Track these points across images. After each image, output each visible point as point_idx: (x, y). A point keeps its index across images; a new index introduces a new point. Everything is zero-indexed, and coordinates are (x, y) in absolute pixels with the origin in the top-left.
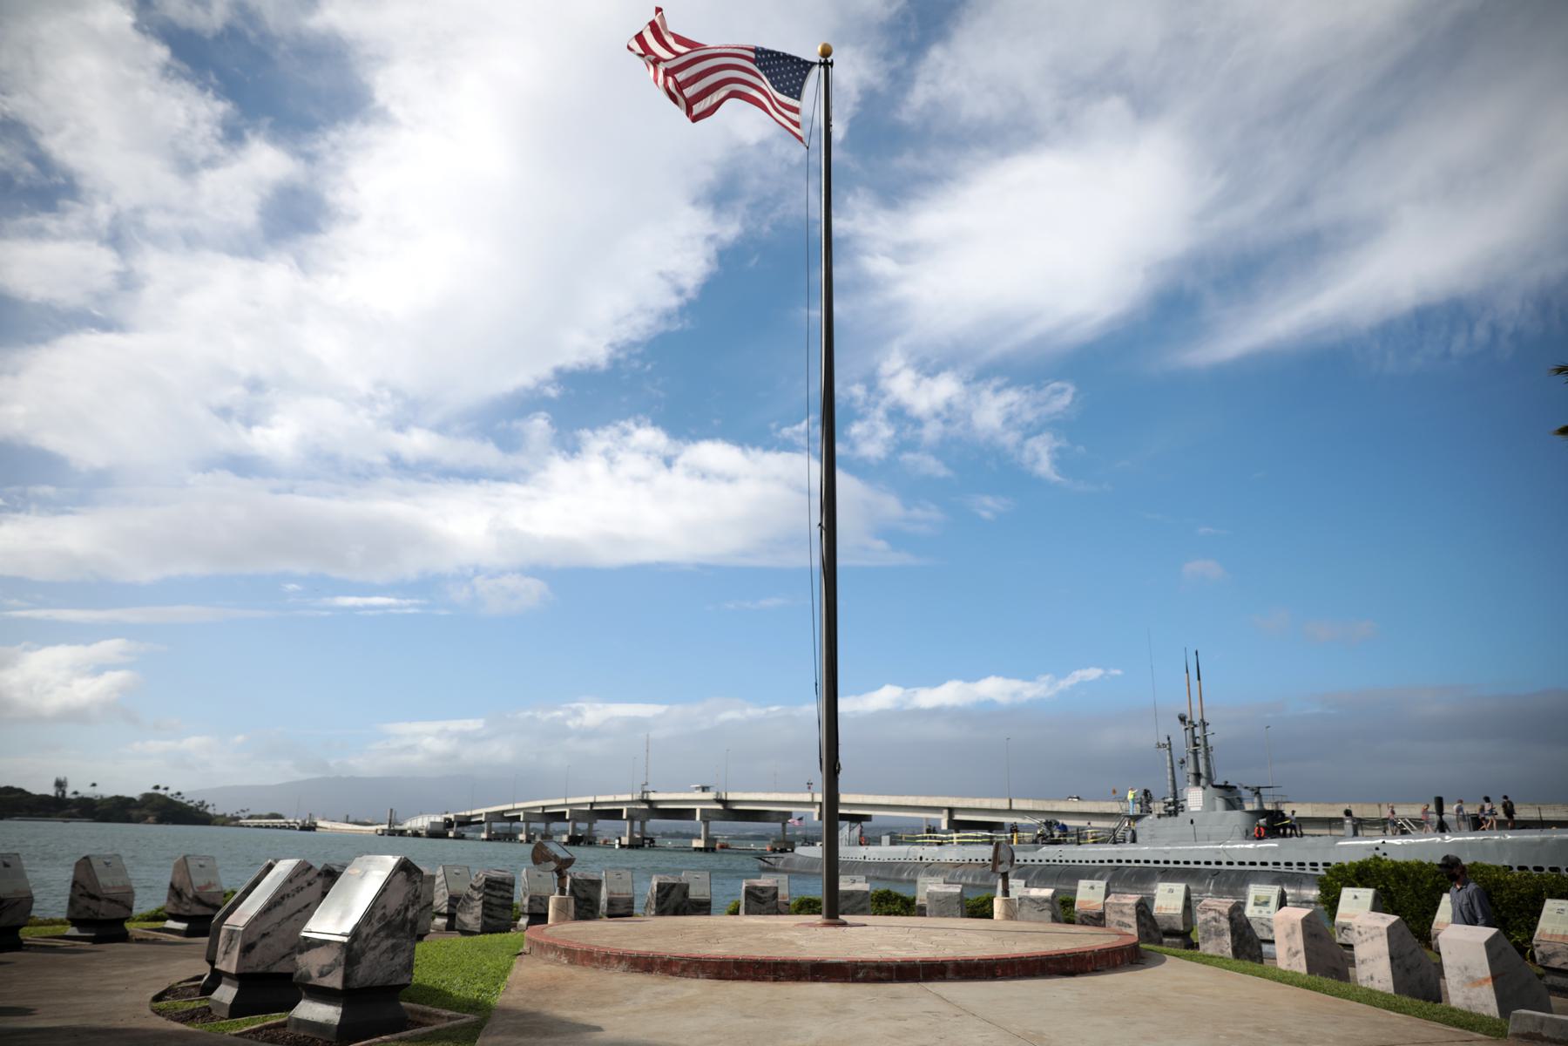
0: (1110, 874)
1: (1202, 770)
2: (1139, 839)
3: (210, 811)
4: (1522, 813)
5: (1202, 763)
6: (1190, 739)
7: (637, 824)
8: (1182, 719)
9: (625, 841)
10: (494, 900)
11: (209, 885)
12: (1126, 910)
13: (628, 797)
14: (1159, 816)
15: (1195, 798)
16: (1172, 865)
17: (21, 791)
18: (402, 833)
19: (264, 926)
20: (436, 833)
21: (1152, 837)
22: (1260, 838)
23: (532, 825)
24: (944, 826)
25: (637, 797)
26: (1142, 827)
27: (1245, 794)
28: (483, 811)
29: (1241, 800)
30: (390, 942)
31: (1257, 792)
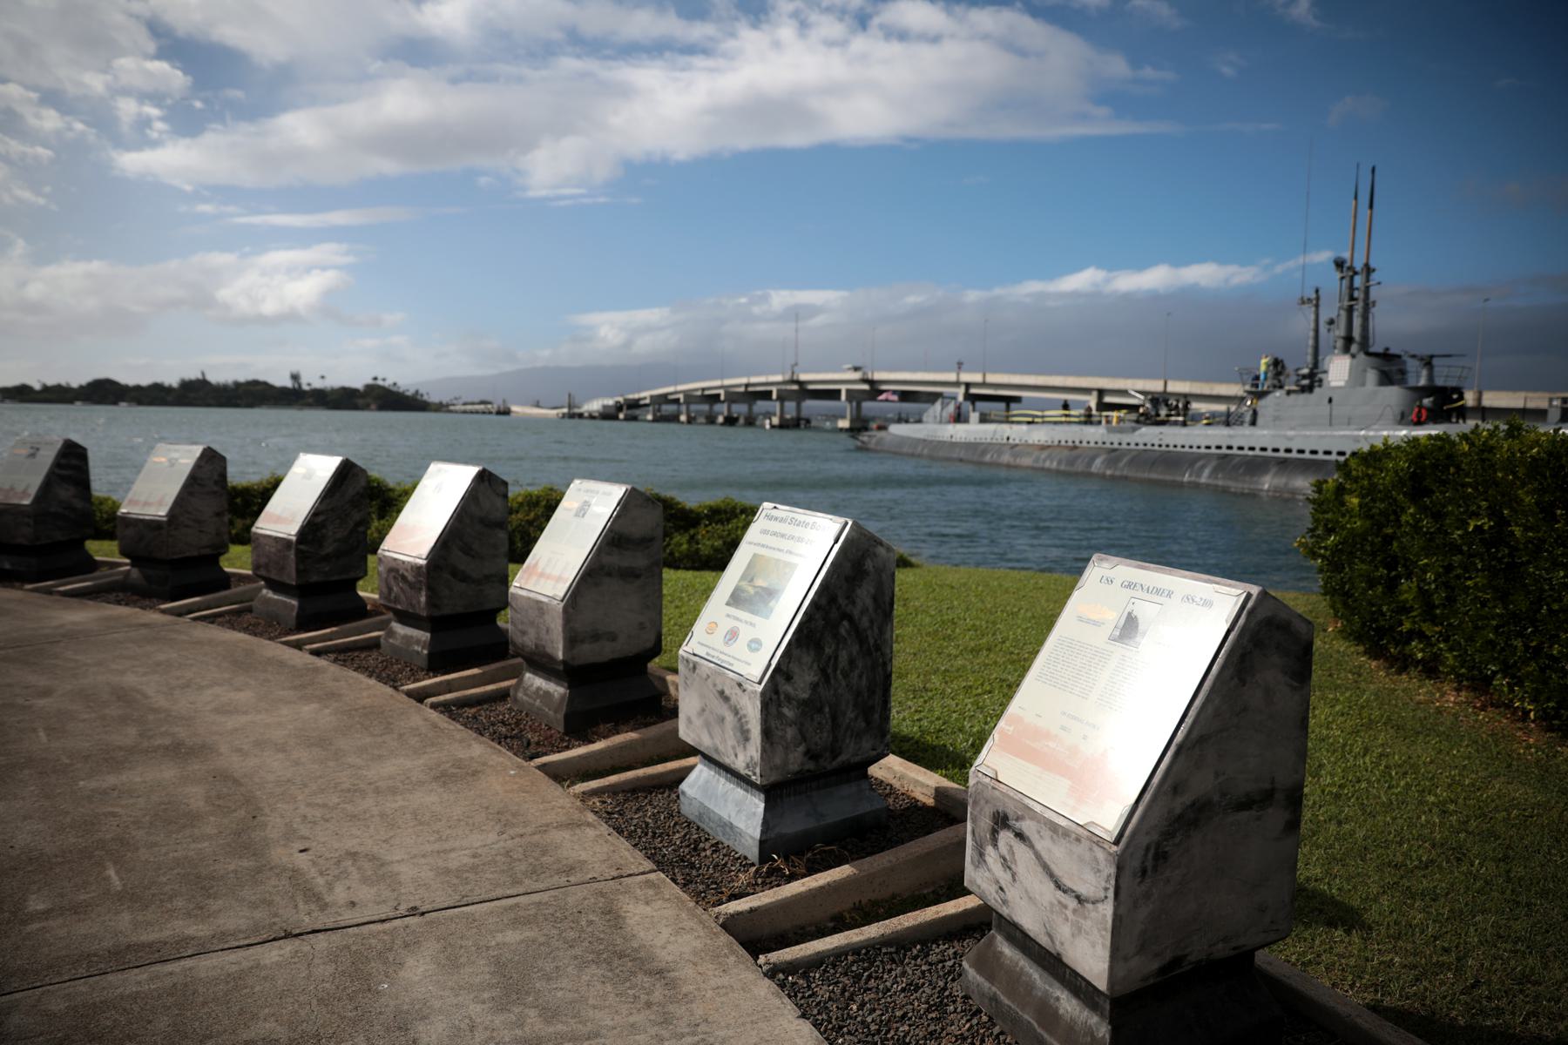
0: (1214, 463)
1: (1356, 333)
2: (1260, 421)
5: (1357, 322)
6: (1345, 291)
8: (1339, 264)
9: (776, 421)
13: (779, 378)
15: (1338, 370)
16: (1294, 455)
17: (265, 384)
18: (581, 416)
20: (608, 415)
21: (1276, 418)
22: (1418, 423)
23: (693, 407)
24: (961, 398)
25: (788, 377)
26: (1267, 406)
27: (1412, 365)
29: (1403, 372)
31: (1428, 362)
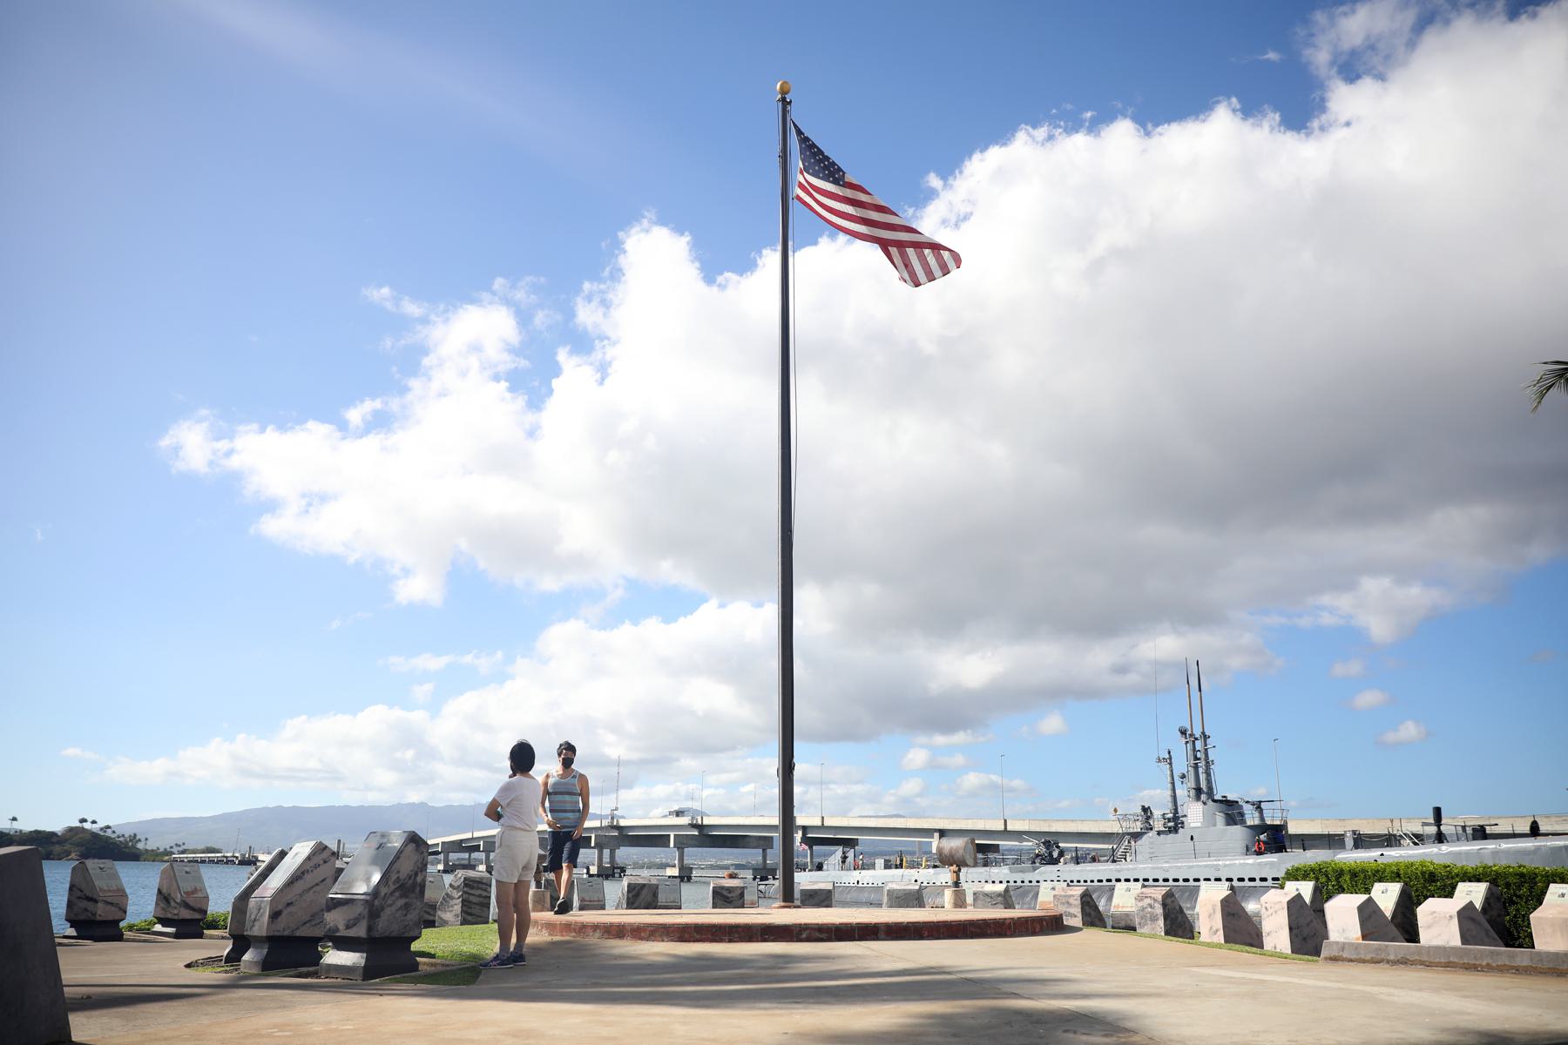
1: (1203, 785)
3: (140, 846)
4: (1543, 828)
5: (1202, 777)
7: (606, 852)
8: (1183, 732)
9: (594, 870)
10: (472, 899)
11: (195, 891)
12: (1071, 901)
14: (1159, 833)
15: (1195, 813)
19: (290, 897)
22: (1259, 853)
25: (605, 823)
28: (439, 840)
29: (1242, 815)
30: (401, 902)
31: (1258, 806)
